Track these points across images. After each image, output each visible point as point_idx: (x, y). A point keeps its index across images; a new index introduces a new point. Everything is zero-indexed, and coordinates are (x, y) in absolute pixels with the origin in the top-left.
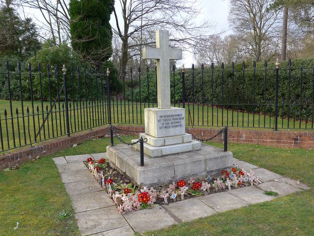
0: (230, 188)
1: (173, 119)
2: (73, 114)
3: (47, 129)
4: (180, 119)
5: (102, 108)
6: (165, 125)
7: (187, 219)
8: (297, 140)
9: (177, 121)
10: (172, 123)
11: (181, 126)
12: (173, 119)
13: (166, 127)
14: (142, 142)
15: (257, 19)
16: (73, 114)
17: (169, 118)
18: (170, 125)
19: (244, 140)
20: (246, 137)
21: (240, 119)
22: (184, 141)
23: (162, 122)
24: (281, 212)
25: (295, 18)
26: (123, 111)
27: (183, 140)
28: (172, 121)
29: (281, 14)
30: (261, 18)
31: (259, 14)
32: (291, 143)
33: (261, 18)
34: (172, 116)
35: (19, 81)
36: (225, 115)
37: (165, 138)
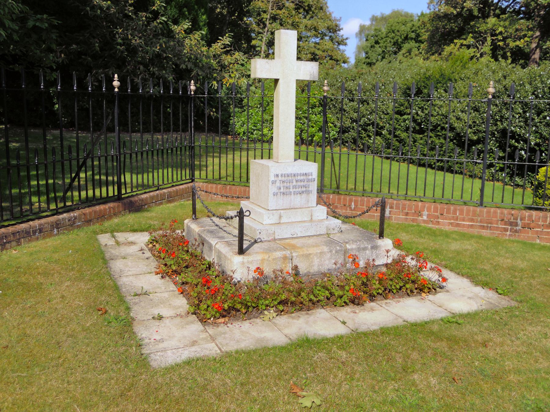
0: (280, 175)
1: (297, 181)
4: (308, 181)
6: (282, 190)
7: (211, 352)
8: (516, 225)
9: (302, 184)
10: (295, 187)
11: (308, 192)
12: (297, 181)
13: (283, 193)
14: (241, 215)
18: (291, 190)
19: (424, 221)
20: (428, 216)
22: (314, 218)
23: (278, 184)
27: (312, 216)
28: (294, 183)
32: (506, 230)
34: (294, 175)
35: (47, 78)
37: (282, 211)
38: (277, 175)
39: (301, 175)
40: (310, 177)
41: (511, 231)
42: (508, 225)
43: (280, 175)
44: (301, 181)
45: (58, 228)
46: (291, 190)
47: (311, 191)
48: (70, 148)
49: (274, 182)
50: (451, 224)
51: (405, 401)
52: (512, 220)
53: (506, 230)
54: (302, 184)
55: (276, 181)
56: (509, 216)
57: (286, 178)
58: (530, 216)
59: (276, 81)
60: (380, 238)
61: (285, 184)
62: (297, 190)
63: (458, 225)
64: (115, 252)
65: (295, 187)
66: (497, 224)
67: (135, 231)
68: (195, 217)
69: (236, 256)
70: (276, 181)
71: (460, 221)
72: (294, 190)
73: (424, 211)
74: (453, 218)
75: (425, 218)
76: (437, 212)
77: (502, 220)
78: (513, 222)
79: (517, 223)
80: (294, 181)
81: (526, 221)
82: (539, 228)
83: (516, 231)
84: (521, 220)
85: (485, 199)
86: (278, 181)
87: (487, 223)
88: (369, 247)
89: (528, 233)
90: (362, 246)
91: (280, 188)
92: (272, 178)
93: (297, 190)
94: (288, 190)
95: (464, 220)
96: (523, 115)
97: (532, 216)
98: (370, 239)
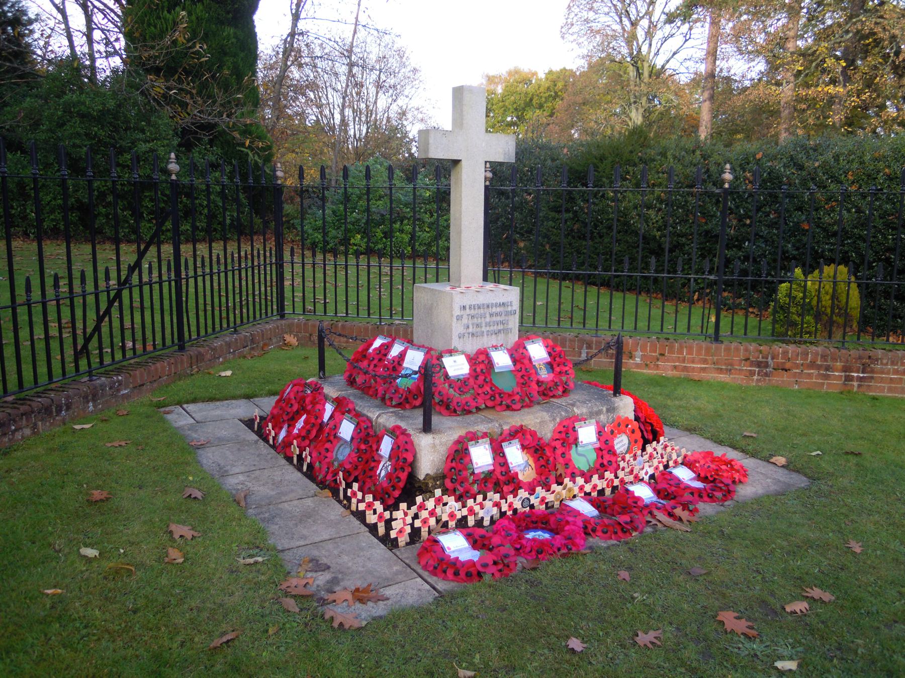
0: (467, 307)
1: (491, 315)
2: (192, 290)
3: (30, 359)
5: (250, 273)
6: (470, 330)
8: (767, 365)
9: (499, 319)
10: (487, 324)
12: (491, 315)
13: (473, 334)
15: (641, 34)
16: (192, 290)
17: (482, 311)
18: (484, 329)
19: (638, 366)
21: (591, 302)
23: (465, 321)
24: (189, 65)
25: (737, 36)
26: (363, 280)
28: (488, 319)
29: (701, 32)
30: (649, 34)
31: (645, 23)
33: (649, 34)
36: (643, 311)
38: (464, 307)
39: (497, 305)
40: (509, 309)
41: (758, 374)
42: (755, 366)
43: (467, 307)
44: (497, 314)
45: (94, 400)
46: (484, 329)
47: (511, 329)
48: (56, 278)
49: (459, 318)
50: (675, 367)
51: (41, 501)
52: (760, 359)
53: (752, 373)
54: (499, 319)
55: (462, 316)
56: (757, 354)
57: (476, 311)
58: (785, 353)
59: (456, 162)
60: (615, 395)
61: (475, 320)
62: (492, 328)
63: (685, 369)
64: (198, 436)
65: (487, 324)
66: (740, 365)
67: (212, 399)
68: (324, 374)
69: (421, 435)
70: (462, 316)
71: (688, 362)
72: (488, 328)
73: (636, 350)
74: (678, 360)
75: (638, 360)
76: (655, 352)
77: (747, 359)
78: (761, 362)
79: (767, 362)
80: (488, 316)
81: (780, 360)
82: (797, 368)
83: (766, 375)
84: (773, 358)
85: (721, 333)
86: (465, 317)
87: (725, 364)
88: (604, 409)
89: (783, 377)
90: (595, 409)
91: (468, 327)
92: (457, 312)
93: (492, 328)
94: (479, 329)
95: (693, 362)
96: (735, 211)
97: (788, 352)
98: (602, 398)
